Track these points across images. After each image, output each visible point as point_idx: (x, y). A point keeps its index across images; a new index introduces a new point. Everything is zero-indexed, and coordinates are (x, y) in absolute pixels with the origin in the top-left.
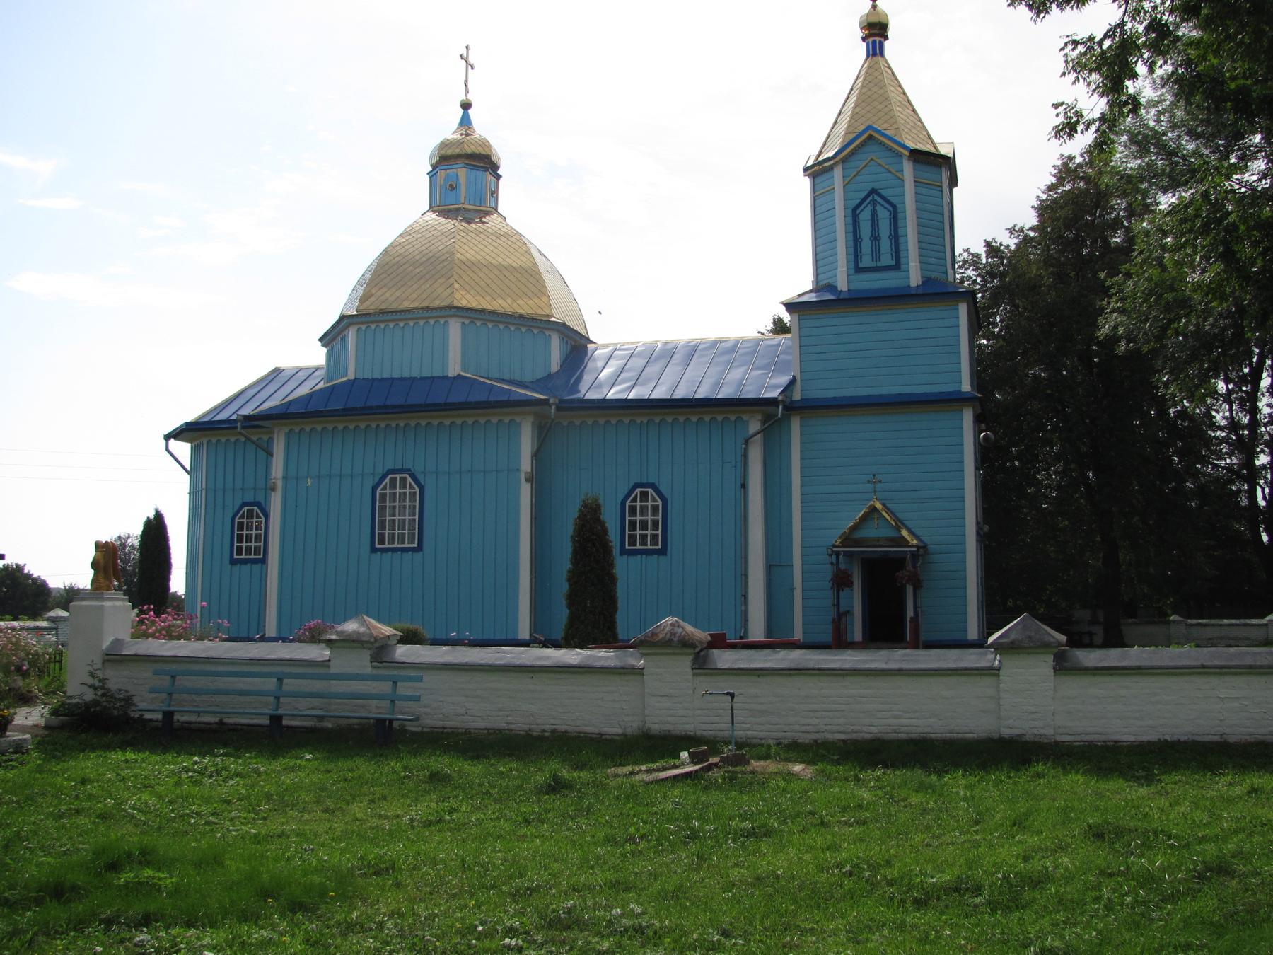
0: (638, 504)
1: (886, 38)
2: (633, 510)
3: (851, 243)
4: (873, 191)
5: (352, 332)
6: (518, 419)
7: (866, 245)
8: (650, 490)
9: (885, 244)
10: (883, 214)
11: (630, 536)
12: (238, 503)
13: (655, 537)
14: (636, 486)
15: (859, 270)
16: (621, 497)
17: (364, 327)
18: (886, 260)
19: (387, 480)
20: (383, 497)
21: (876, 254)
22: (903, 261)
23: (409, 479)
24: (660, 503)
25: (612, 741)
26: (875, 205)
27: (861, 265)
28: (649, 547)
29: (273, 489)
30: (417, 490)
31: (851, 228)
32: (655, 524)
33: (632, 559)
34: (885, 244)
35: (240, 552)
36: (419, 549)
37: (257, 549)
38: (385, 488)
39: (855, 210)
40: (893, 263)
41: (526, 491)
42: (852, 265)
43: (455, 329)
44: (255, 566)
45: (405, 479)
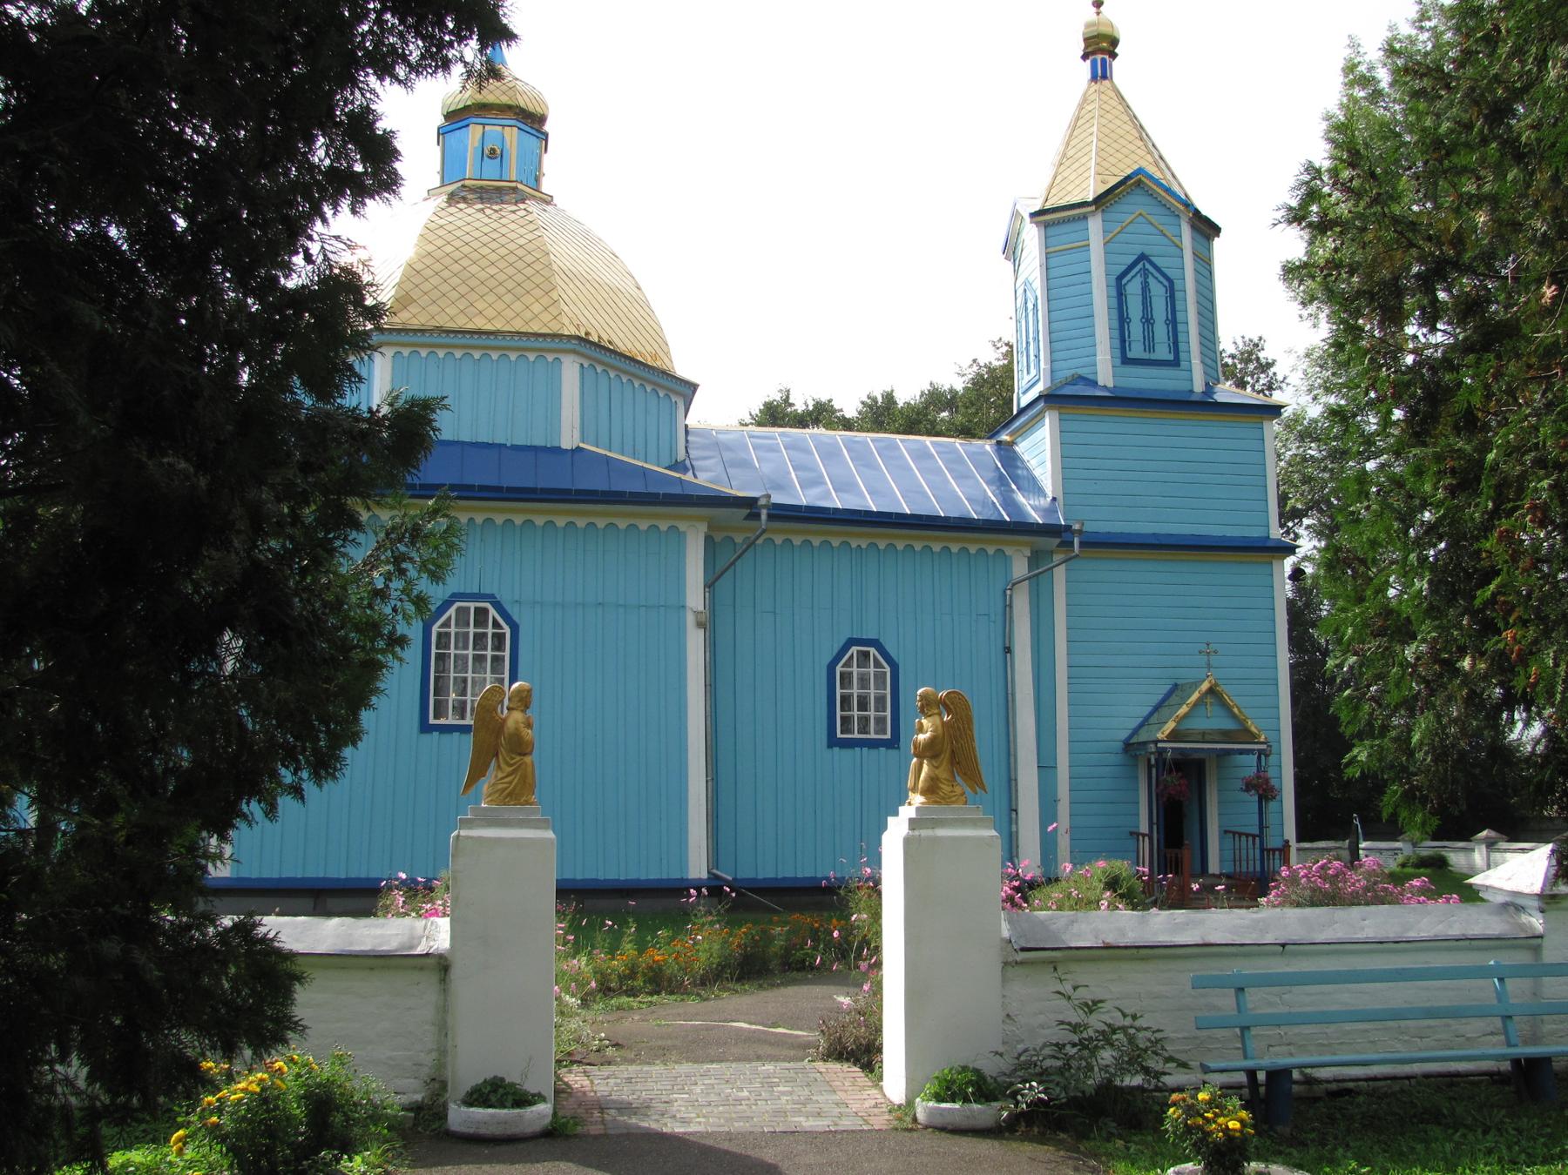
0: (855, 670)
1: (1114, 56)
3: (1116, 324)
4: (1143, 257)
6: (682, 526)
7: (1136, 329)
8: (872, 650)
9: (1161, 331)
10: (1157, 290)
13: (880, 721)
15: (1126, 361)
16: (828, 659)
17: (406, 352)
18: (1162, 353)
19: (452, 611)
20: (443, 639)
21: (1149, 343)
23: (493, 612)
24: (888, 670)
25: (1495, 1077)
26: (1146, 277)
27: (1130, 355)
28: (873, 736)
30: (507, 630)
31: (1114, 302)
32: (880, 701)
34: (1161, 331)
38: (447, 624)
39: (1120, 278)
40: (1171, 357)
41: (695, 642)
42: (1118, 353)
43: (570, 370)
45: (486, 611)
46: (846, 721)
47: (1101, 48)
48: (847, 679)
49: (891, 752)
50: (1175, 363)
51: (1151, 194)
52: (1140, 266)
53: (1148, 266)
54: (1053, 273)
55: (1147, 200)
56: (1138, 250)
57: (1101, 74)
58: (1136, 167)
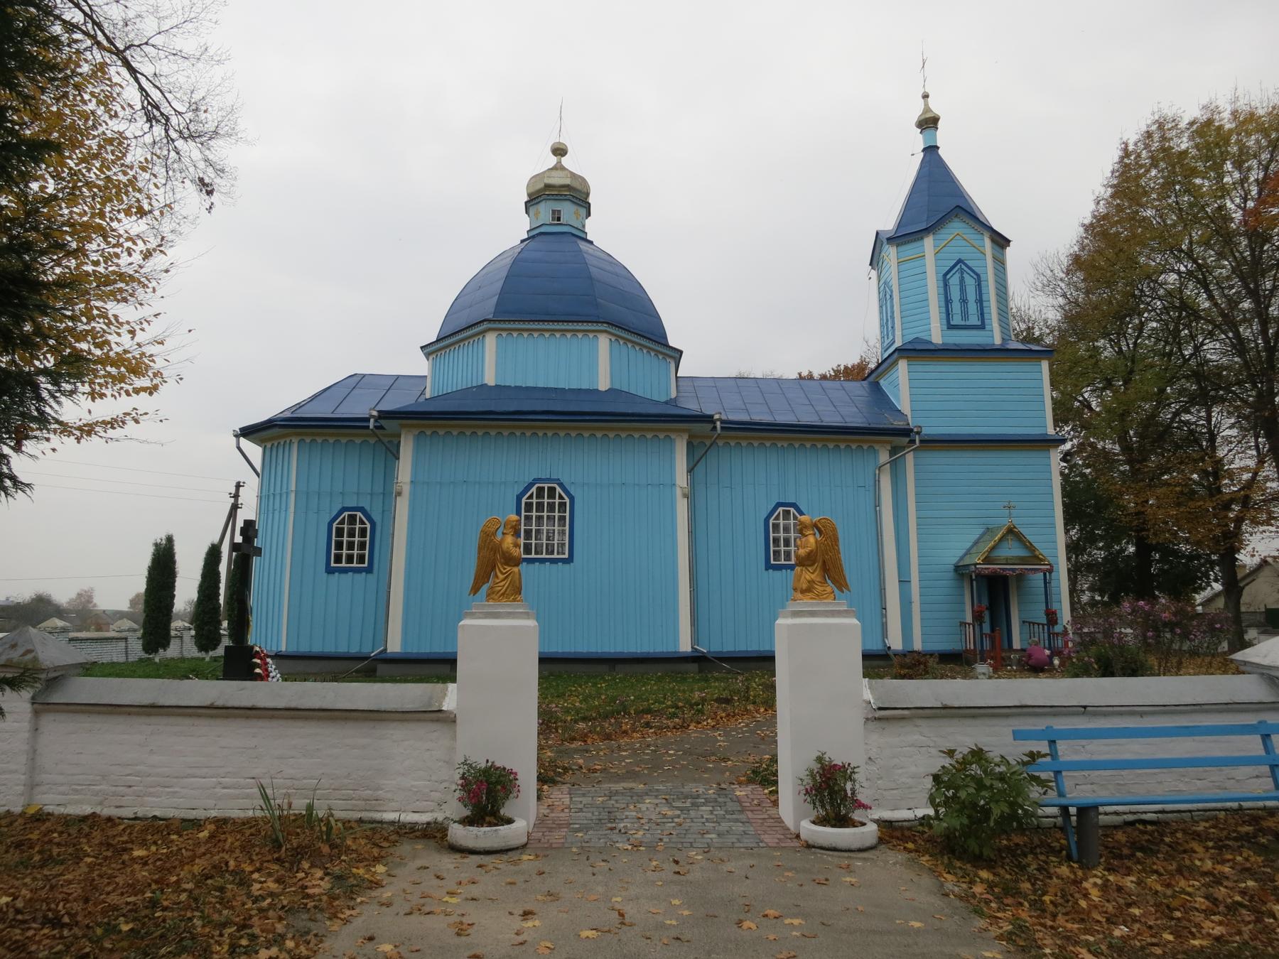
0: (781, 522)
2: (776, 527)
3: (943, 304)
5: (903, 365)
7: (956, 307)
8: (792, 510)
10: (970, 282)
11: (336, 555)
12: (339, 507)
14: (779, 505)
15: (951, 327)
18: (974, 320)
19: (534, 489)
21: (965, 315)
22: (987, 322)
23: (558, 489)
29: (399, 494)
31: (942, 291)
33: (778, 574)
34: (972, 307)
35: (338, 559)
36: (570, 560)
37: (361, 559)
41: (682, 507)
42: (945, 322)
44: (357, 576)
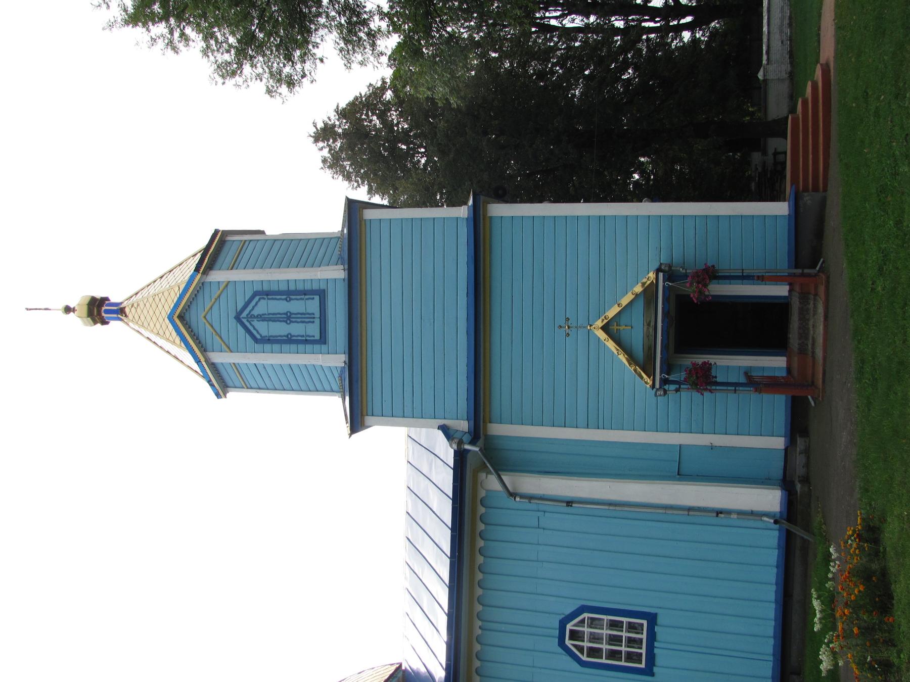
0: (586, 644)
3: (293, 347)
4: (238, 318)
7: (296, 329)
8: (569, 627)
9: (296, 306)
10: (263, 307)
15: (323, 339)
16: (575, 666)
18: (313, 306)
21: (305, 318)
26: (253, 317)
27: (317, 337)
31: (276, 347)
32: (614, 625)
34: (296, 306)
39: (256, 340)
40: (317, 298)
46: (630, 657)
47: (98, 310)
48: (593, 652)
49: (660, 620)
50: (322, 294)
51: (188, 306)
52: (245, 321)
53: (244, 314)
54: (262, 385)
55: (193, 307)
56: (233, 322)
57: (120, 311)
58: (167, 321)
